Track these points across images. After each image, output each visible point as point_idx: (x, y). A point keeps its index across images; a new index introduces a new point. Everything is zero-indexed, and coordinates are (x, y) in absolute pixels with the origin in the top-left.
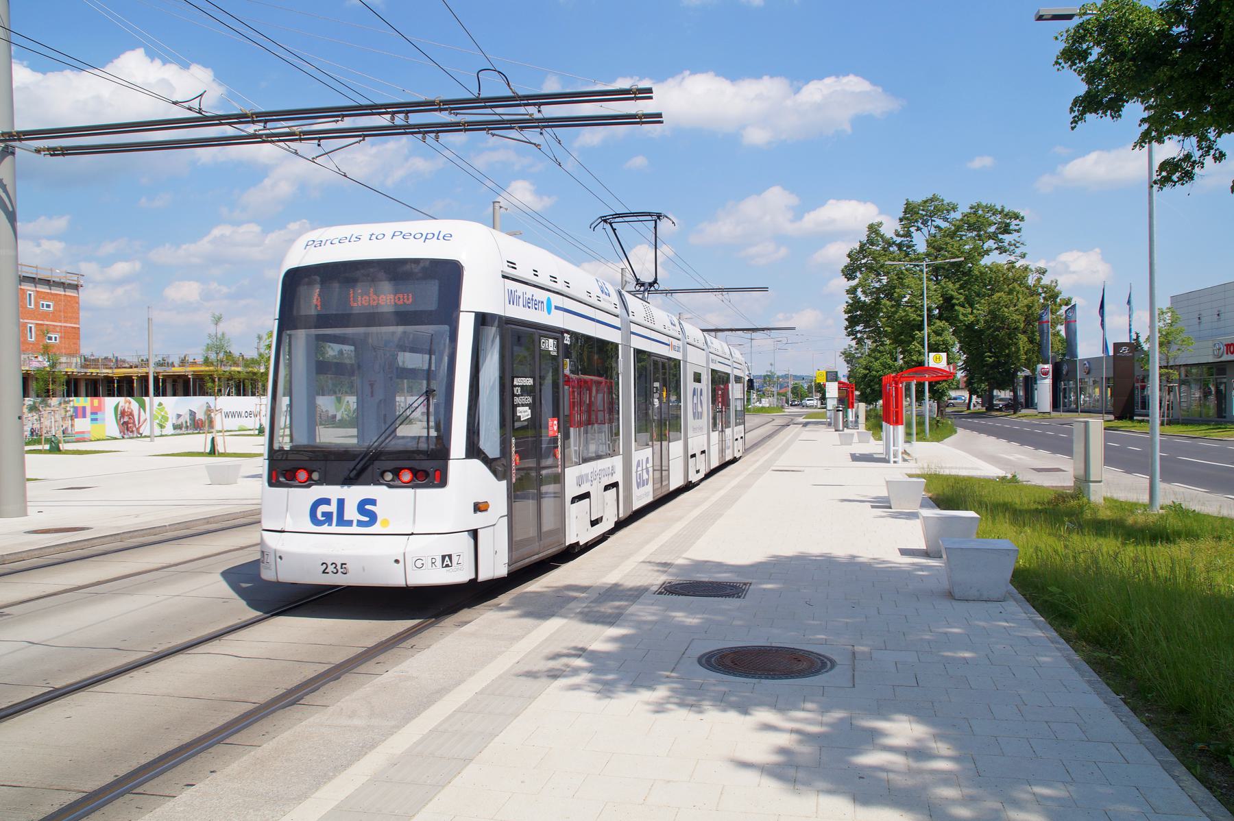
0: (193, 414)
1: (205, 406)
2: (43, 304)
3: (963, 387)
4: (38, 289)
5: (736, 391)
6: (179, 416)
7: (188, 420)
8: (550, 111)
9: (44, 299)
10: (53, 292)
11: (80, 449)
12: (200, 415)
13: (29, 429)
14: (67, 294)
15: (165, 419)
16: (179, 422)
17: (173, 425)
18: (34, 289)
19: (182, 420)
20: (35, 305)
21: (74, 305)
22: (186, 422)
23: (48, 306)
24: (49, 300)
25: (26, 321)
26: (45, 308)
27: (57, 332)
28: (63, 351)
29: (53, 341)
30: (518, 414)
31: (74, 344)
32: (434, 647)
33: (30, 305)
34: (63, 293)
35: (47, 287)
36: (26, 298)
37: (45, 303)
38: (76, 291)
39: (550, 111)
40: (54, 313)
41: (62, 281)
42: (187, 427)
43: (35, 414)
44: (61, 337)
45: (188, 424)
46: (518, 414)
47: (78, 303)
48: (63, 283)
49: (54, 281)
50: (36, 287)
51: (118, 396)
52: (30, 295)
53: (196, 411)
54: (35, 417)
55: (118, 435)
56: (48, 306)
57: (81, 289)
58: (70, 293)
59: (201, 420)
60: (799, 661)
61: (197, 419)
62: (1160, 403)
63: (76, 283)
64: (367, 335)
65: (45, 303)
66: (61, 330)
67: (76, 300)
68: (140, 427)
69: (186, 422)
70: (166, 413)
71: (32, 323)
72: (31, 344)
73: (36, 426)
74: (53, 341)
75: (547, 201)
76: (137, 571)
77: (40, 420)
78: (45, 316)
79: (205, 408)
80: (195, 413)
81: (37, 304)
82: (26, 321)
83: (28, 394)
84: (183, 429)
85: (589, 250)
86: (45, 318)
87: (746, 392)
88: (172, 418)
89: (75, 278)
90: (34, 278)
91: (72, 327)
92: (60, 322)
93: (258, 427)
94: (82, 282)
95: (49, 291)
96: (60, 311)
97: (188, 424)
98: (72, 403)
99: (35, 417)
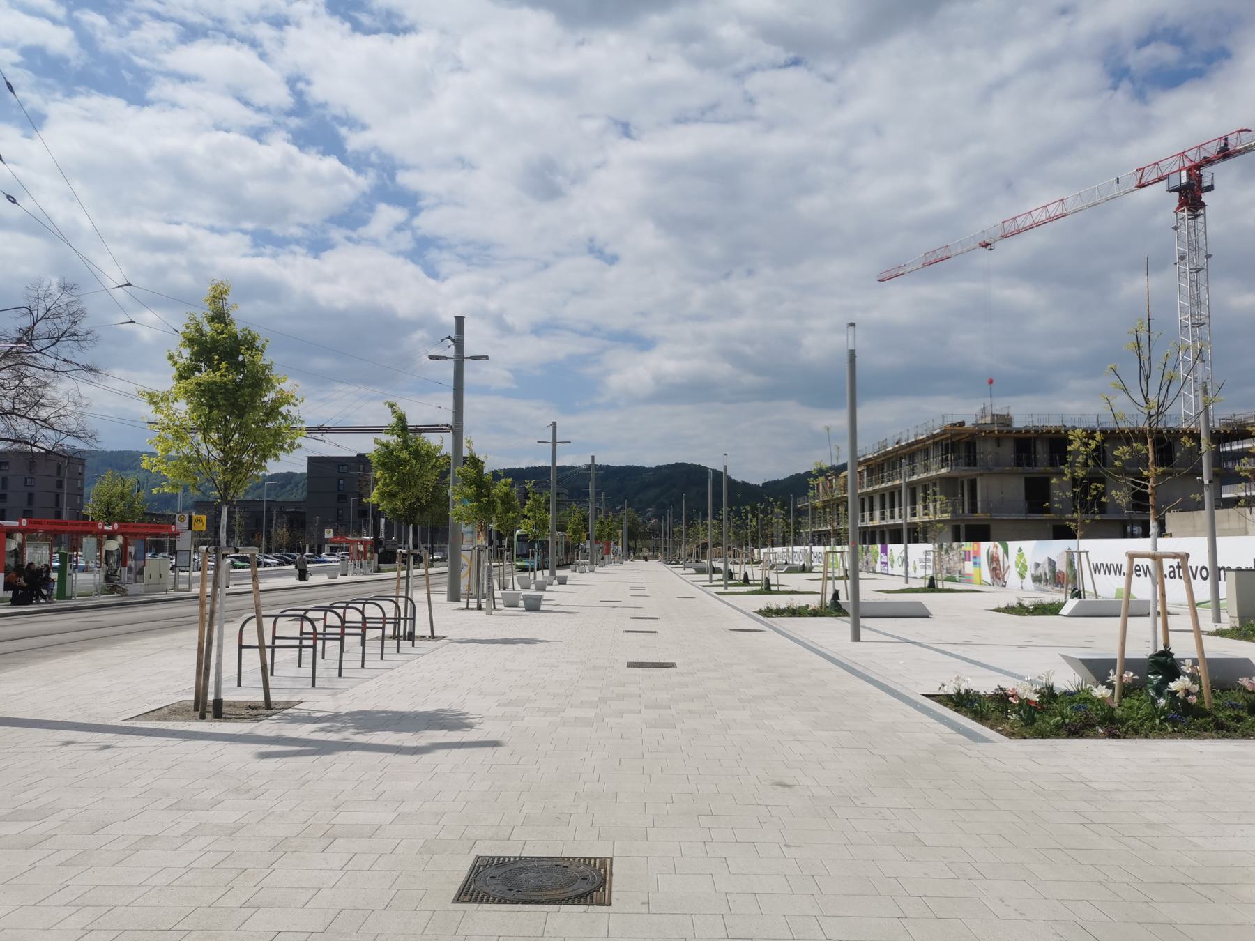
0: (1052, 563)
6: (1037, 565)
7: (1047, 571)
8: (269, 662)
12: (1061, 566)
15: (1024, 567)
16: (1038, 574)
17: (1032, 575)
19: (1040, 571)
22: (1046, 574)
30: (988, 420)
32: (135, 450)
39: (269, 662)
42: (1047, 580)
45: (1048, 578)
46: (988, 420)
53: (1055, 560)
55: (990, 581)
59: (1061, 572)
60: (1016, 910)
61: (1057, 571)
68: (1004, 575)
69: (1046, 574)
70: (1024, 560)
73: (948, 566)
75: (25, 584)
76: (1002, 668)
80: (1055, 563)
84: (1042, 582)
85: (87, 620)
88: (1031, 568)
93: (391, 420)
97: (1048, 578)
98: (963, 548)
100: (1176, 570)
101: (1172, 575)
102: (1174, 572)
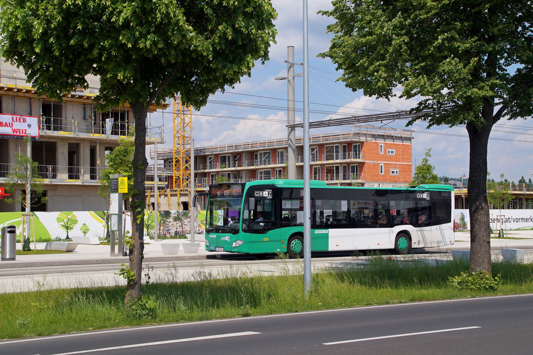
1: (460, 214)
2: (389, 151)
3: (113, 216)
4: (386, 142)
5: (409, 252)
9: (389, 148)
10: (395, 143)
11: (514, 237)
13: (174, 232)
14: (404, 144)
18: (384, 142)
20: (384, 152)
21: (408, 150)
23: (392, 152)
24: (393, 148)
25: (379, 162)
26: (390, 154)
27: (397, 168)
28: (401, 180)
29: (395, 174)
31: (409, 175)
33: (381, 152)
34: (401, 143)
35: (383, 139)
36: (378, 148)
37: (390, 150)
38: (410, 142)
40: (395, 156)
41: (392, 135)
43: (178, 222)
44: (400, 171)
47: (411, 149)
48: (402, 137)
49: (395, 136)
50: (385, 141)
51: (519, 209)
52: (381, 146)
54: (178, 225)
56: (392, 152)
57: (412, 140)
58: (406, 143)
62: (358, 186)
63: (410, 136)
64: (88, 131)
65: (390, 150)
66: (399, 166)
67: (409, 147)
71: (382, 163)
72: (382, 176)
73: (179, 230)
74: (395, 174)
77: (182, 226)
78: (390, 158)
79: (460, 216)
81: (385, 151)
82: (379, 162)
83: (15, 210)
86: (390, 159)
87: (345, 261)
89: (409, 133)
90: (384, 135)
91: (407, 165)
92: (399, 161)
94: (413, 136)
95: (393, 143)
96: (399, 155)
99: (178, 225)
100: (508, 220)
101: (507, 221)
102: (507, 220)
